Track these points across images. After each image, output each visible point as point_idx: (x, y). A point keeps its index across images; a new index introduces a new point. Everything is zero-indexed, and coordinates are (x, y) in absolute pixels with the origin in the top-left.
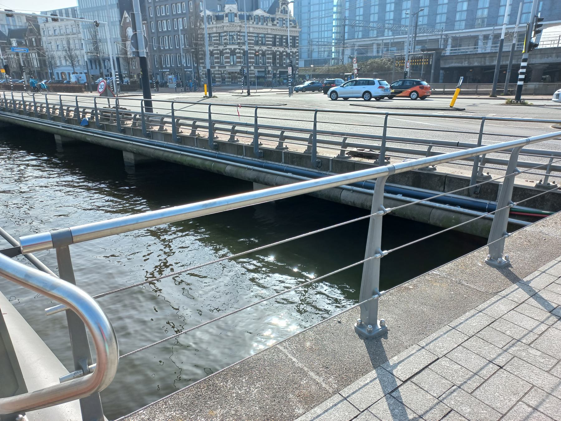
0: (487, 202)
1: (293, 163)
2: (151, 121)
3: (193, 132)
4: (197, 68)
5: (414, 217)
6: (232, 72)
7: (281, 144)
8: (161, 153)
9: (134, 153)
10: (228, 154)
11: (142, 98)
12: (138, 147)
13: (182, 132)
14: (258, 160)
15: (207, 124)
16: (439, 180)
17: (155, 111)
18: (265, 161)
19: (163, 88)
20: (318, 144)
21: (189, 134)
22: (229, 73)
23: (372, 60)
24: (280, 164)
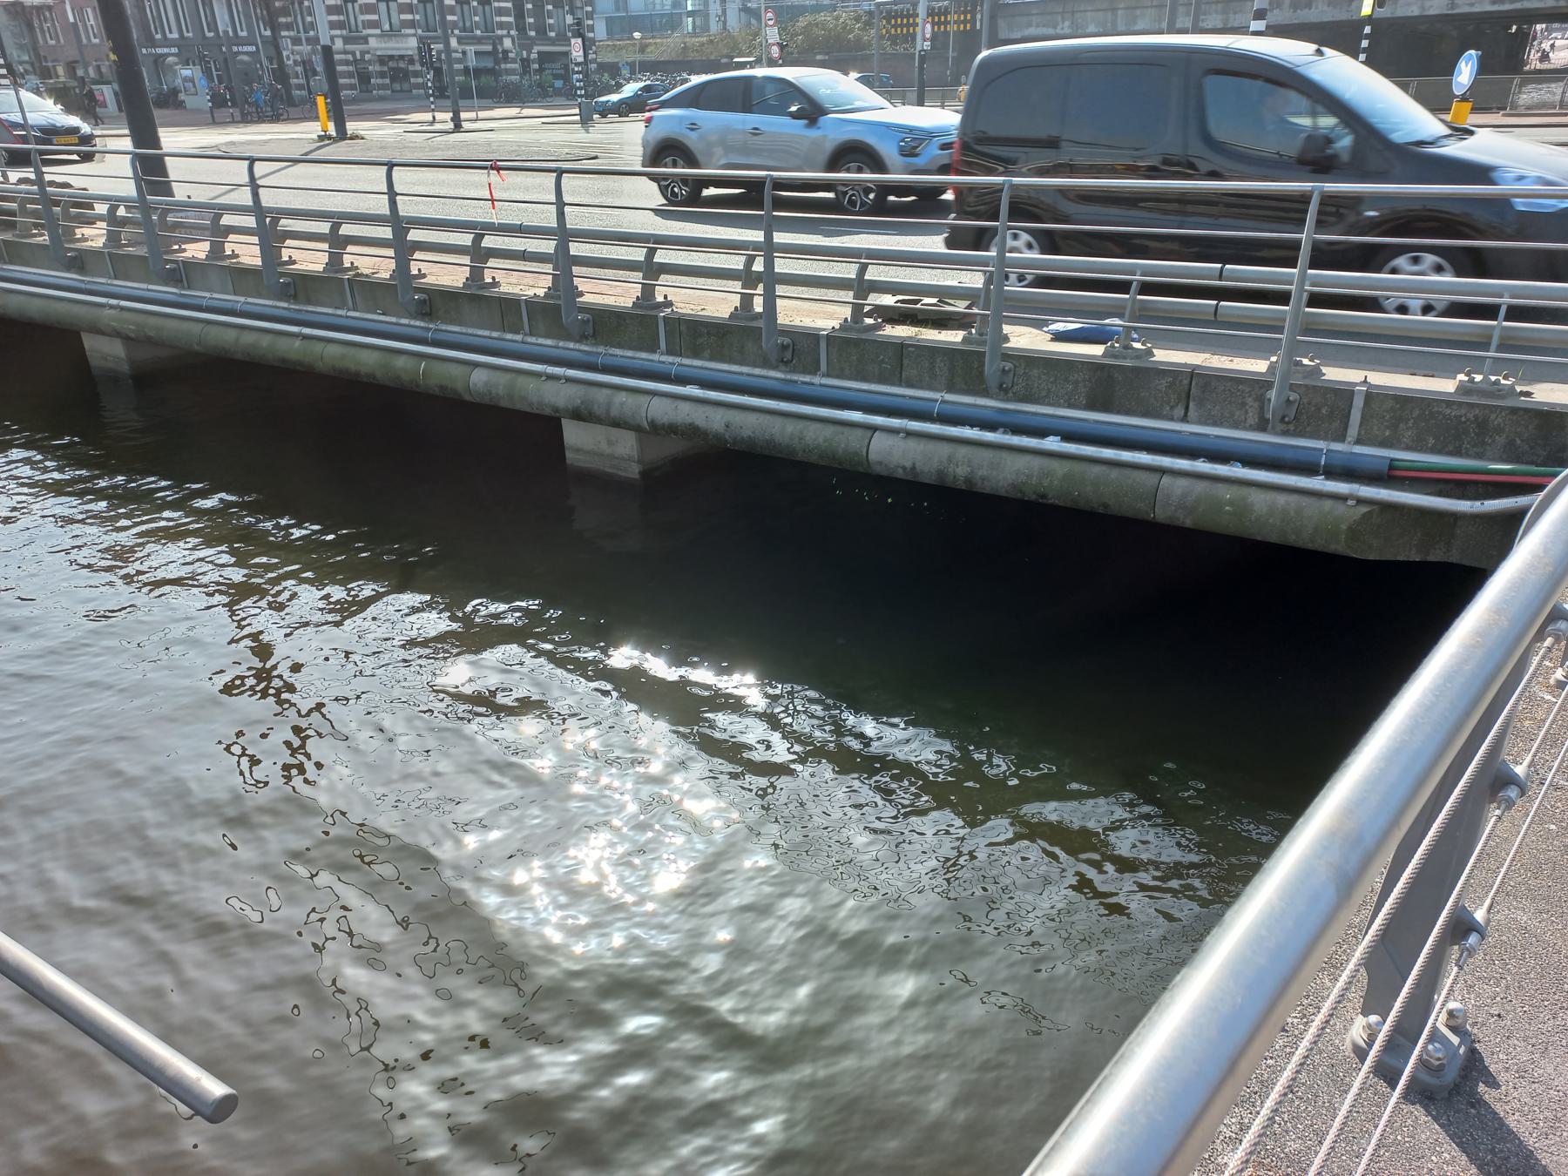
0: (1320, 444)
1: (696, 354)
2: (177, 226)
3: (335, 261)
4: (274, 43)
5: (1106, 506)
6: (391, 57)
7: (648, 291)
8: (230, 335)
9: (637, 429)
10: (470, 331)
11: (127, 144)
12: (141, 318)
13: (292, 262)
14: (577, 346)
15: (386, 232)
16: (1171, 385)
17: (180, 192)
18: (601, 349)
19: (165, 112)
20: (576, 270)
21: (320, 268)
22: (382, 60)
23: (809, 18)
24: (656, 357)
